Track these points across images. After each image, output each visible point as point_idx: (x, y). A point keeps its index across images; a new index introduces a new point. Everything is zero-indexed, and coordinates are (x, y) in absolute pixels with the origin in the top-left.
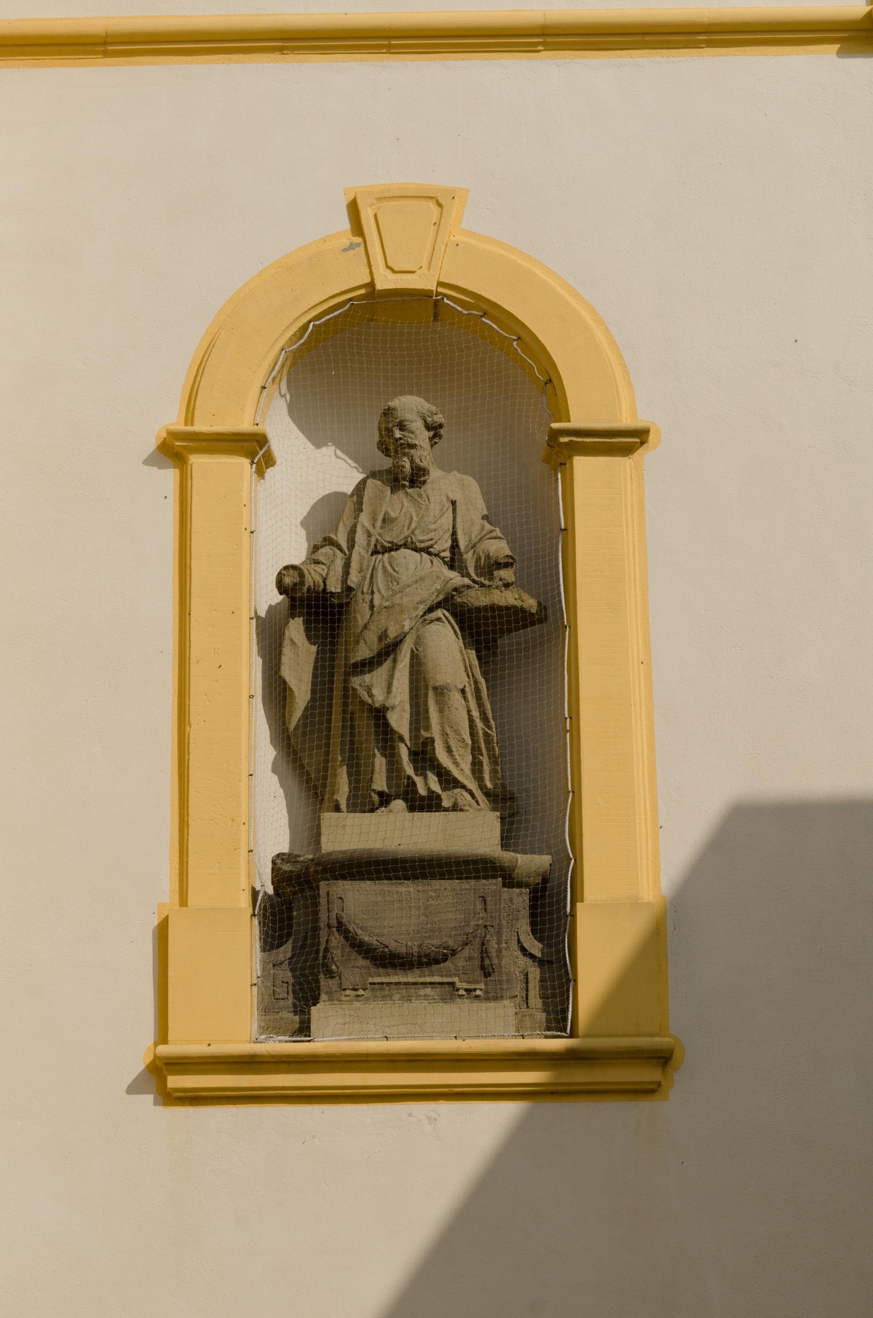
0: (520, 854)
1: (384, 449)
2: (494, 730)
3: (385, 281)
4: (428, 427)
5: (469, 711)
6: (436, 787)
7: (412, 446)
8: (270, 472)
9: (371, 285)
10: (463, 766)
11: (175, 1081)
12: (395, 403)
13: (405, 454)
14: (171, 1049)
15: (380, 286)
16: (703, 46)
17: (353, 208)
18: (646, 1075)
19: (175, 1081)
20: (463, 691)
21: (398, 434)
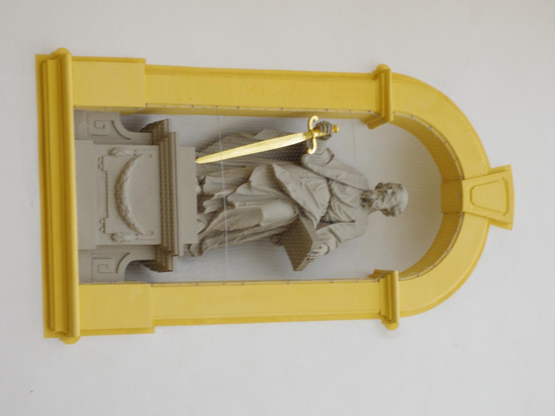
0: (228, 245)
1: (379, 186)
2: (237, 243)
3: (466, 186)
4: (392, 209)
5: (247, 229)
6: (207, 211)
7: (383, 200)
8: (365, 128)
9: (464, 179)
10: (219, 225)
11: (51, 66)
12: (405, 190)
13: (378, 196)
14: (70, 66)
15: (464, 183)
16: (426, 267)
17: (500, 170)
18: (59, 327)
19: (51, 66)
20: (258, 225)
21: (390, 191)
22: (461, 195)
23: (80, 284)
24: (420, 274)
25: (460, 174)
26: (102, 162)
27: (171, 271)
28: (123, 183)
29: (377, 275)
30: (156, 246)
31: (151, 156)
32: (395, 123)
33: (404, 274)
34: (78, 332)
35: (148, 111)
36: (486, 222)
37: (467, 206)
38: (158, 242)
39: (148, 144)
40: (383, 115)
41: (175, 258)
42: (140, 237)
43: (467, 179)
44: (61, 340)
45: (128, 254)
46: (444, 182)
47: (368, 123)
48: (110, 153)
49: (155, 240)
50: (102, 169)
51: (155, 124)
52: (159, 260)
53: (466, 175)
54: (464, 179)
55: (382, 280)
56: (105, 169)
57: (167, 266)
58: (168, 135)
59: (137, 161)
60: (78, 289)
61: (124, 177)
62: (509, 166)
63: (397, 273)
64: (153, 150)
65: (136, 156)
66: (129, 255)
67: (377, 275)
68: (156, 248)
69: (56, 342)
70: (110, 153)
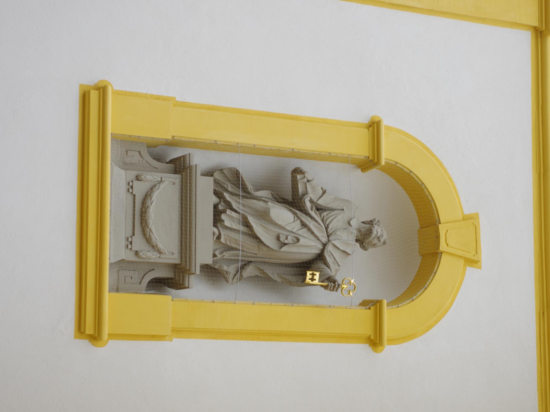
3: (442, 229)
9: (440, 223)
18: (89, 329)
22: (438, 237)
23: (109, 292)
24: (414, 298)
25: (437, 218)
26: (132, 187)
27: (188, 288)
28: (148, 207)
29: (365, 304)
30: (176, 265)
31: (174, 184)
32: (384, 169)
33: (396, 302)
34: (105, 336)
35: (173, 143)
36: (462, 262)
37: (443, 247)
38: (177, 261)
39: (171, 173)
40: (376, 161)
41: (192, 277)
42: (162, 256)
43: (442, 224)
44: (90, 341)
45: (154, 269)
46: (421, 228)
47: (361, 168)
48: (138, 178)
49: (175, 259)
50: (132, 193)
51: (178, 159)
52: (177, 278)
53: (442, 220)
54: (440, 223)
55: (372, 308)
56: (134, 193)
57: (183, 284)
58: (190, 167)
59: (162, 186)
60: (107, 296)
61: (149, 203)
62: (477, 214)
63: (385, 302)
64: (176, 178)
65: (161, 181)
66: (154, 270)
67: (365, 304)
68: (175, 267)
69: (85, 343)
70: (138, 178)
